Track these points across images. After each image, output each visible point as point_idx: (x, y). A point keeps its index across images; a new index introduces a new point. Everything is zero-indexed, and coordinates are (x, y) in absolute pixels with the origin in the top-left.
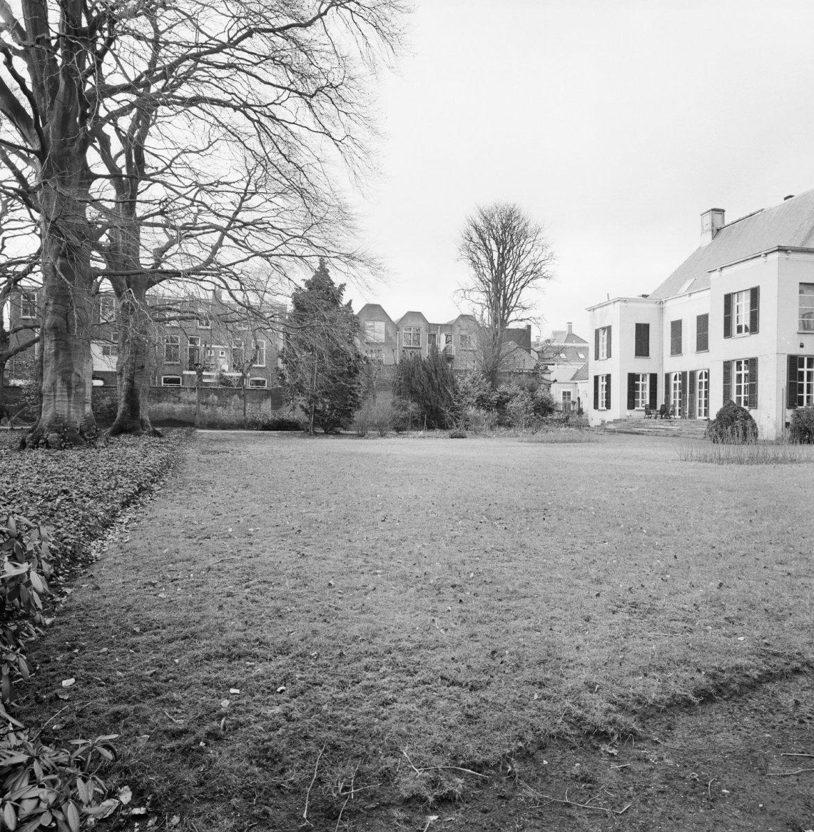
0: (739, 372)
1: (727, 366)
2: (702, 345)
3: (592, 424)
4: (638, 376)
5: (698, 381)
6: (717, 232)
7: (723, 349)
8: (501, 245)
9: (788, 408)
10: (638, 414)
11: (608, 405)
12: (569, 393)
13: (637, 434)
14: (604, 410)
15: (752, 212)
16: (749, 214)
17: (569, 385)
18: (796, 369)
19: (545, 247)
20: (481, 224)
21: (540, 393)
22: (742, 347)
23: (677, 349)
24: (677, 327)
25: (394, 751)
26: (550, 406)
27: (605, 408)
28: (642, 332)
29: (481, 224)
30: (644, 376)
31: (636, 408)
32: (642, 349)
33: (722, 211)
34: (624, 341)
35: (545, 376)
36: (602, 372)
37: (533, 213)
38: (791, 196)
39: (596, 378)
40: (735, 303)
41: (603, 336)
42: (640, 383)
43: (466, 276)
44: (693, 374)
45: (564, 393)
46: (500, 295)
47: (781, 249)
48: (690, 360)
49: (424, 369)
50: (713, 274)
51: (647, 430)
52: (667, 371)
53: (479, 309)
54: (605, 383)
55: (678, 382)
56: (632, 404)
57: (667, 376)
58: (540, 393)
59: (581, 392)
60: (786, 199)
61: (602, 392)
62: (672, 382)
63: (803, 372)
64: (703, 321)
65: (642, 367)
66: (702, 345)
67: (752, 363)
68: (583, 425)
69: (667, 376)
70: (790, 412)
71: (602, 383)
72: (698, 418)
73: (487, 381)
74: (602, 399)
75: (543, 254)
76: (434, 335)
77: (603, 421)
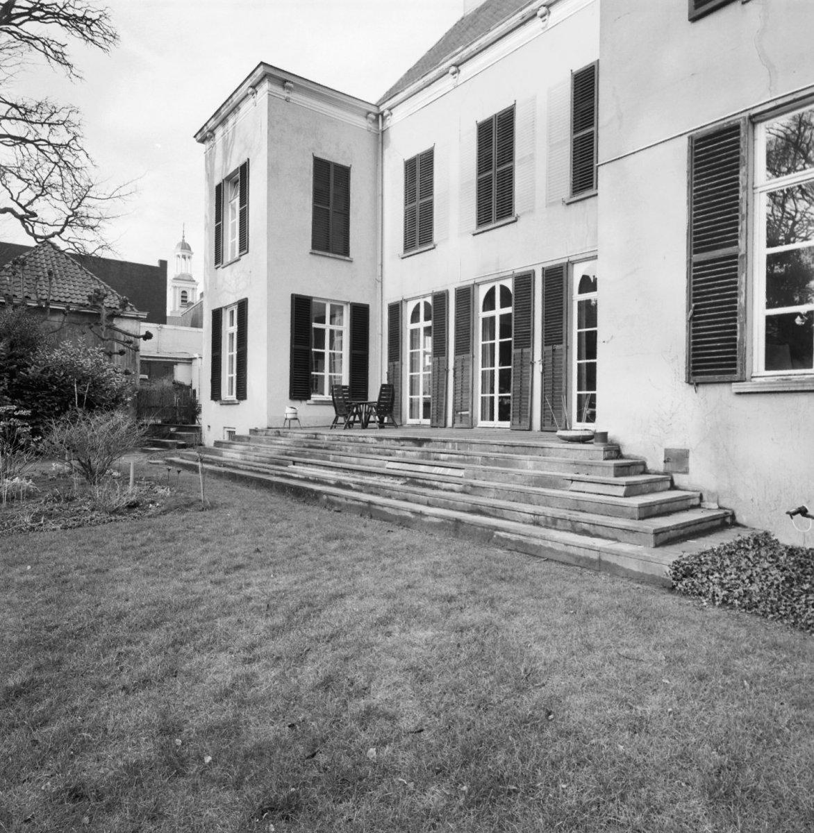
0: (489, 314)
5: (481, 315)
10: (317, 412)
18: (434, 323)
23: (419, 231)
25: (163, 643)
27: (234, 397)
28: (331, 185)
30: (336, 310)
34: (282, 208)
36: (229, 299)
44: (465, 295)
51: (331, 475)
52: (391, 297)
55: (423, 324)
57: (395, 311)
61: (229, 353)
62: (408, 326)
64: (497, 137)
65: (328, 281)
69: (395, 310)
71: (229, 328)
74: (228, 374)
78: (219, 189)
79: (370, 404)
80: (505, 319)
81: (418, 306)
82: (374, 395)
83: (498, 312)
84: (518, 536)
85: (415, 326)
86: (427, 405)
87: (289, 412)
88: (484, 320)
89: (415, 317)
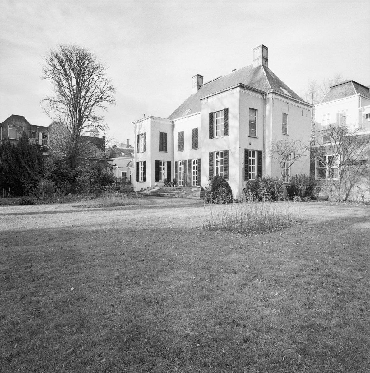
1: (211, 155)
2: (195, 145)
3: (136, 190)
4: (161, 162)
6: (199, 87)
7: (207, 146)
8: (76, 71)
9: (245, 180)
11: (144, 180)
12: (125, 173)
13: (161, 196)
14: (142, 182)
15: (217, 77)
16: (215, 78)
17: (125, 169)
19: (107, 81)
20: (62, 56)
21: (104, 172)
22: (220, 143)
23: (181, 146)
24: (181, 135)
26: (110, 180)
27: (143, 181)
28: (163, 137)
29: (62, 56)
31: (160, 181)
32: (163, 147)
33: (202, 77)
34: (152, 142)
35: (110, 162)
36: (141, 160)
37: (99, 55)
38: (236, 70)
39: (138, 163)
40: (216, 118)
41: (142, 140)
42: (162, 166)
43: (49, 89)
44: (190, 161)
45: (123, 173)
46: (77, 106)
47: (242, 86)
48: (188, 154)
49: (12, 152)
50: (203, 102)
53: (63, 115)
54: (143, 166)
56: (157, 178)
57: (176, 163)
58: (104, 172)
59: (132, 173)
60: (233, 71)
61: (141, 171)
62: (179, 166)
63: (251, 159)
64: (195, 133)
65: (163, 157)
66: (195, 145)
67: (225, 154)
68: (129, 191)
69: (176, 163)
70: (245, 182)
71: (141, 166)
72: (193, 186)
73: (67, 163)
75: (106, 86)
76: (34, 133)
77: (142, 189)
78: (138, 136)
79: (172, 182)
80: (197, 166)
81: (195, 161)
82: (172, 180)
83: (196, 165)
84: (69, 112)
85: (194, 165)
86: (183, 182)
87: (156, 184)
88: (193, 166)
89: (194, 164)
